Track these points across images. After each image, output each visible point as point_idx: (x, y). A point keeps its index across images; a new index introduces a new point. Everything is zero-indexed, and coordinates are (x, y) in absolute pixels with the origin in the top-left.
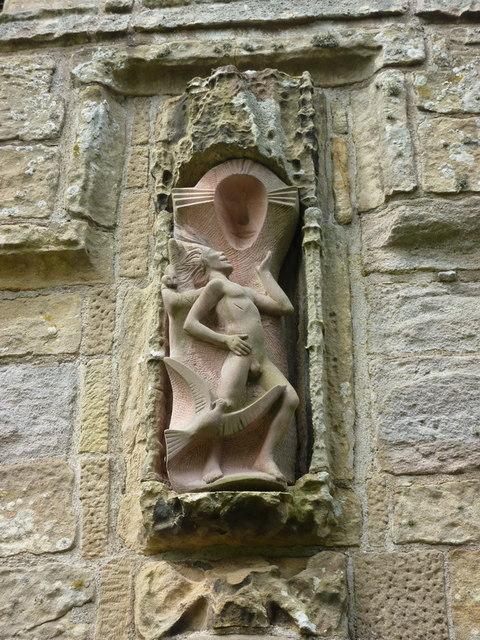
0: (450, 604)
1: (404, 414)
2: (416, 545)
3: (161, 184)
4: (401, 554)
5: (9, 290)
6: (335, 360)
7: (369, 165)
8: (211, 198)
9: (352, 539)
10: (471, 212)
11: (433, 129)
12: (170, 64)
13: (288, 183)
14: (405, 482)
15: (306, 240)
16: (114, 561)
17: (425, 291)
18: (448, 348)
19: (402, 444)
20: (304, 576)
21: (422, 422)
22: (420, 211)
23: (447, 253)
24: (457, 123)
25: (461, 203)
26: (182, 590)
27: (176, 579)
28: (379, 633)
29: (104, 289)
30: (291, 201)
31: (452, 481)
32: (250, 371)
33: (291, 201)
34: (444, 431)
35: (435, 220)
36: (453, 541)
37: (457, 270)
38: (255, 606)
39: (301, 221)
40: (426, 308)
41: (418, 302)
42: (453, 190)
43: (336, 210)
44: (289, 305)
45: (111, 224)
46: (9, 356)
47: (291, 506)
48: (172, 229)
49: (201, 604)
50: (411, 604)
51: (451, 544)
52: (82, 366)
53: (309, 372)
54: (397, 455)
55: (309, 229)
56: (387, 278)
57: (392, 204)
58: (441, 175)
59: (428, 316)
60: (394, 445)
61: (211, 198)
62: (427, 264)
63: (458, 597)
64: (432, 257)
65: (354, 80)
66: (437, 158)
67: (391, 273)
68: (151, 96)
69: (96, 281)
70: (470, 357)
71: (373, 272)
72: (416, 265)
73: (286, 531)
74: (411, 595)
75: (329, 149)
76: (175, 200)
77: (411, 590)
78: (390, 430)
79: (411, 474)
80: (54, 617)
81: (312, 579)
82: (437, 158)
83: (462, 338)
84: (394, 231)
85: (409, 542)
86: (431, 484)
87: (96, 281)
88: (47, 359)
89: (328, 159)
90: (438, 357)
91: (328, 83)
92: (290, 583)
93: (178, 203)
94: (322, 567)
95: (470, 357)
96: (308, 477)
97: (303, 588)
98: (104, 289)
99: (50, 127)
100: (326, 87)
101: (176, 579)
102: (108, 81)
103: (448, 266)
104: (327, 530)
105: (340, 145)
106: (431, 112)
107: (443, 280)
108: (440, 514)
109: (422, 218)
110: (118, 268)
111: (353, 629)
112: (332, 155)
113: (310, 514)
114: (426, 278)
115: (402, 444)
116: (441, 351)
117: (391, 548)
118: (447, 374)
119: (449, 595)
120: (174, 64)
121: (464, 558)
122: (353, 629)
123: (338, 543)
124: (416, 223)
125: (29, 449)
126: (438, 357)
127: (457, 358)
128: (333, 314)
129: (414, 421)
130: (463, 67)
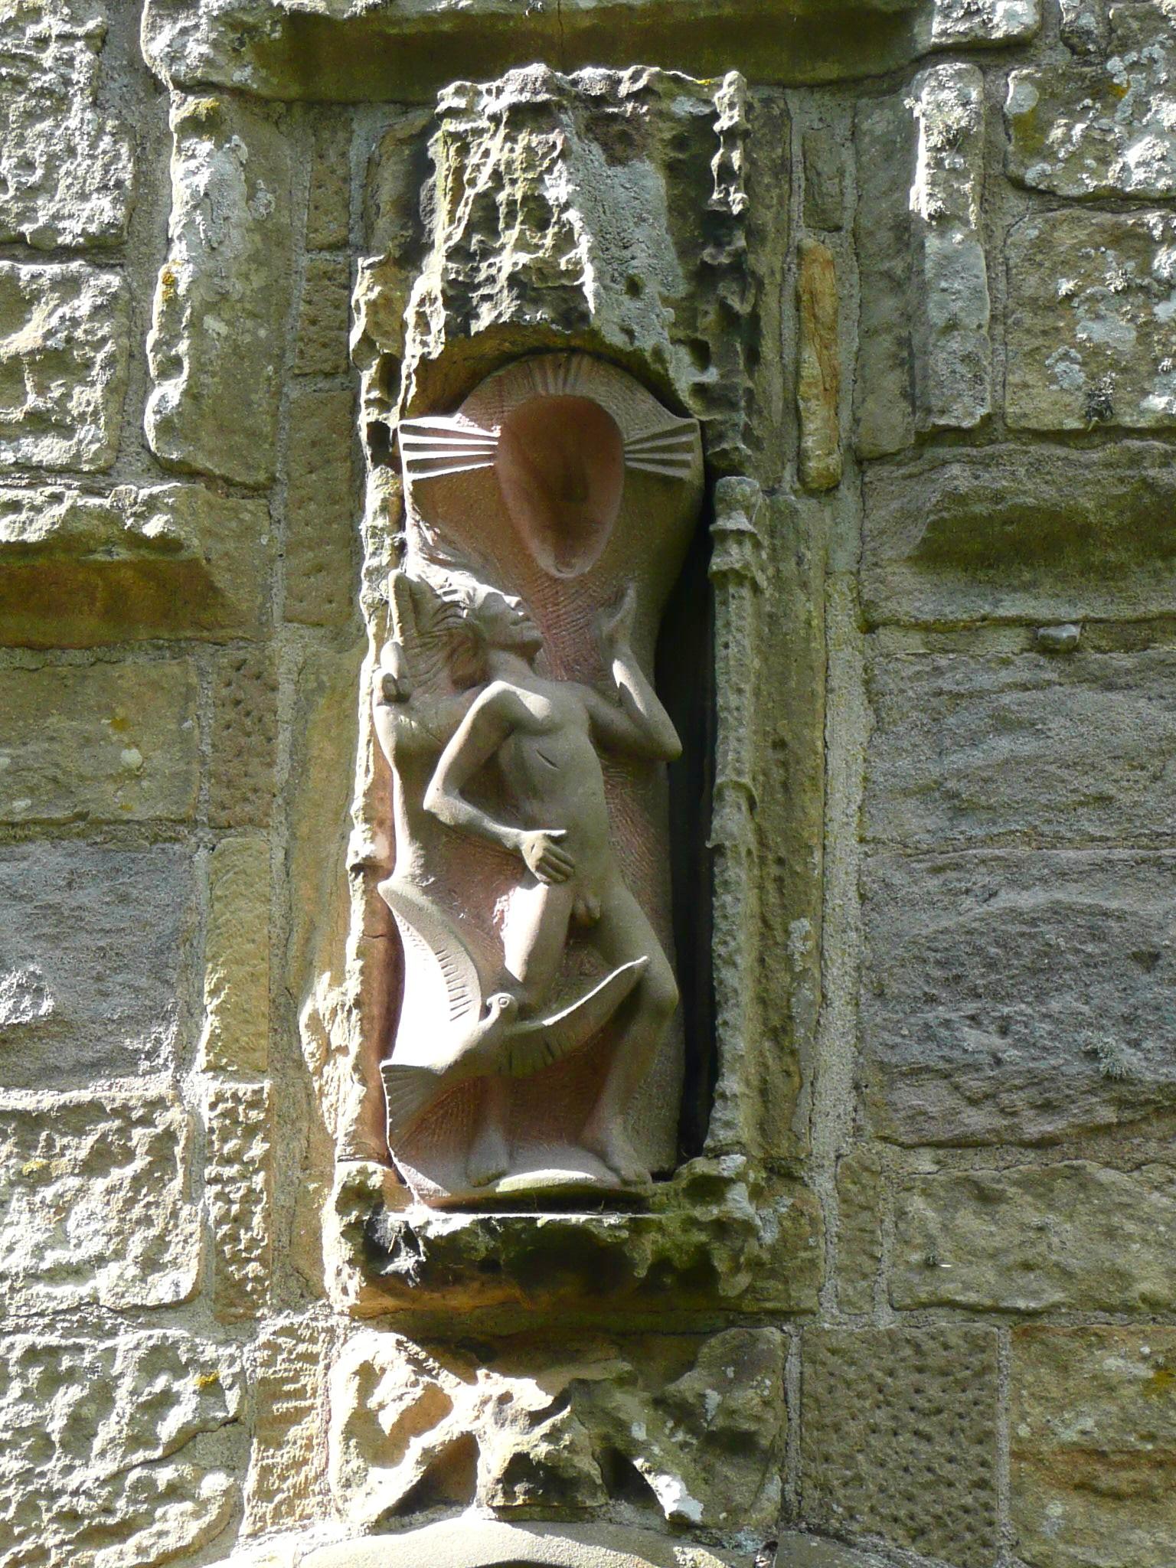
0: (1005, 1445)
1: (932, 1000)
2: (941, 1312)
3: (375, 394)
4: (908, 1333)
5: (29, 646)
6: (780, 861)
7: (889, 329)
8: (489, 458)
9: (805, 1297)
10: (1121, 480)
11: (1043, 244)
12: (393, 31)
13: (680, 410)
14: (924, 1162)
15: (717, 563)
16: (289, 1331)
17: (1005, 676)
18: (1046, 829)
19: (916, 1072)
20: (689, 1384)
21: (972, 1018)
22: (995, 479)
23: (1062, 578)
24: (1102, 228)
25: (1096, 456)
26: (432, 1409)
27: (415, 1384)
28: (849, 1509)
29: (250, 654)
30: (685, 464)
31: (1029, 1163)
32: (573, 917)
33: (685, 464)
34: (1021, 1042)
35: (1030, 501)
36: (1021, 1304)
37: (1083, 623)
38: (576, 1460)
39: (707, 507)
40: (1004, 724)
41: (984, 708)
42: (1073, 424)
43: (801, 456)
44: (672, 740)
45: (261, 477)
46: (35, 822)
47: (659, 1237)
48: (400, 523)
49: (465, 1449)
50: (923, 1447)
51: (1017, 1312)
52: (202, 855)
53: (711, 907)
54: (908, 1096)
55: (725, 534)
56: (915, 642)
57: (929, 453)
58: (1053, 379)
59: (1003, 745)
60: (903, 1074)
61: (489, 458)
62: (1012, 606)
63: (1024, 1431)
64: (1026, 587)
65: (862, 69)
66: (1044, 333)
67: (926, 628)
68: (355, 104)
69: (231, 632)
70: (1100, 853)
71: (885, 624)
72: (986, 609)
73: (651, 1285)
74: (923, 1426)
75: (791, 280)
76: (403, 439)
77: (926, 1414)
78: (899, 1040)
79: (939, 1145)
80: (158, 1453)
81: (703, 1396)
82: (1044, 333)
83: (1081, 804)
84: (933, 527)
85: (925, 1306)
86: (982, 1168)
87: (231, 632)
88: (121, 831)
89: (789, 310)
90: (1023, 851)
91: (800, 77)
92: (659, 1403)
93: (414, 465)
94: (727, 1365)
95: (1100, 853)
96: (701, 1166)
97: (684, 1413)
98: (250, 654)
99: (104, 209)
100: (796, 86)
101: (415, 1384)
102: (240, 75)
103: (1064, 611)
104: (743, 1280)
105: (816, 270)
106: (1042, 193)
107: (1048, 649)
108: (997, 1242)
109: (998, 497)
110: (279, 596)
111: (792, 1497)
112: (798, 299)
113: (703, 1254)
114: (1009, 642)
115: (916, 1072)
116: (1033, 836)
117: (886, 1320)
118: (1029, 900)
119: (1002, 1425)
120: (408, 30)
121: (1043, 1342)
122: (792, 1497)
123: (769, 1305)
124: (980, 509)
125: (88, 1055)
126: (1023, 851)
127: (1067, 855)
128: (780, 745)
129: (953, 1016)
130: (1133, 56)
